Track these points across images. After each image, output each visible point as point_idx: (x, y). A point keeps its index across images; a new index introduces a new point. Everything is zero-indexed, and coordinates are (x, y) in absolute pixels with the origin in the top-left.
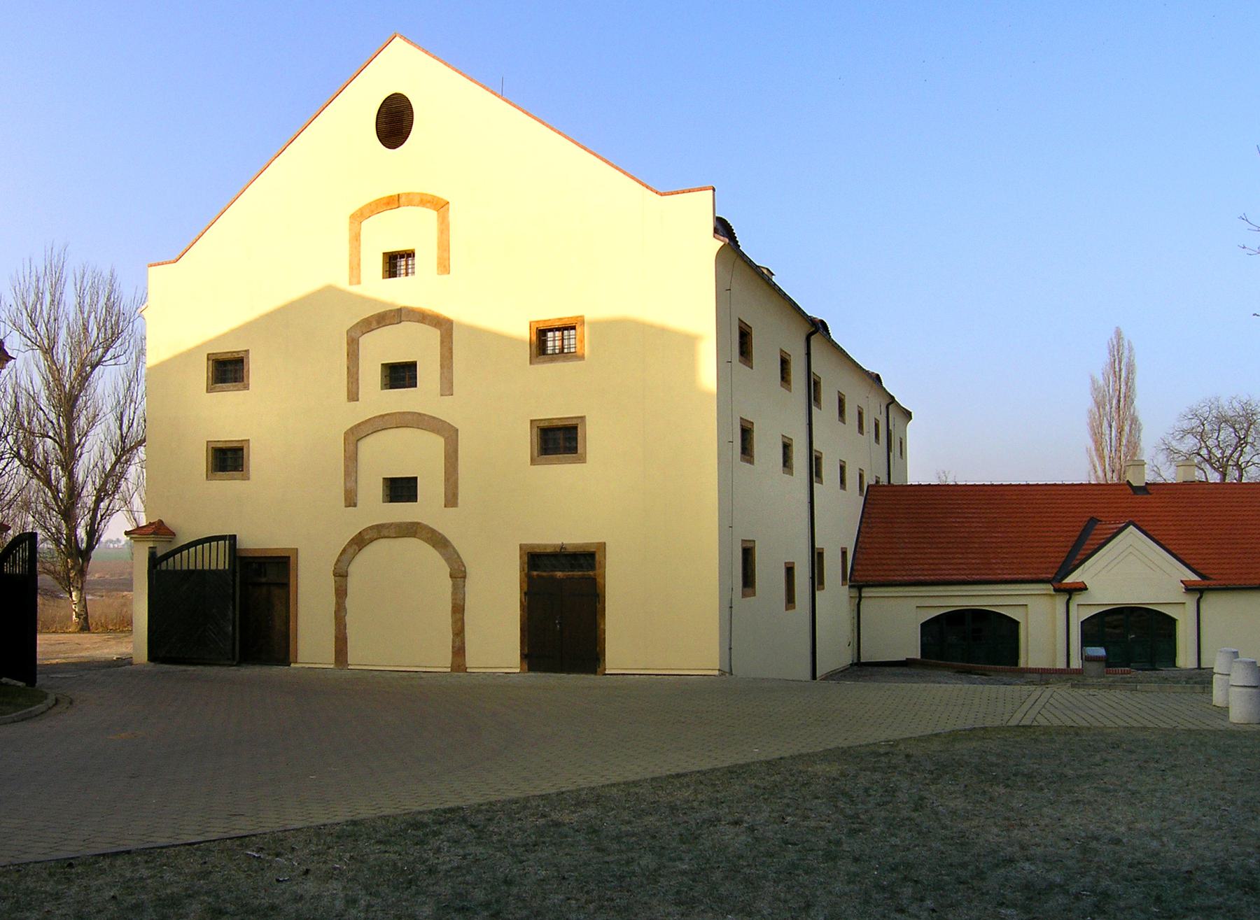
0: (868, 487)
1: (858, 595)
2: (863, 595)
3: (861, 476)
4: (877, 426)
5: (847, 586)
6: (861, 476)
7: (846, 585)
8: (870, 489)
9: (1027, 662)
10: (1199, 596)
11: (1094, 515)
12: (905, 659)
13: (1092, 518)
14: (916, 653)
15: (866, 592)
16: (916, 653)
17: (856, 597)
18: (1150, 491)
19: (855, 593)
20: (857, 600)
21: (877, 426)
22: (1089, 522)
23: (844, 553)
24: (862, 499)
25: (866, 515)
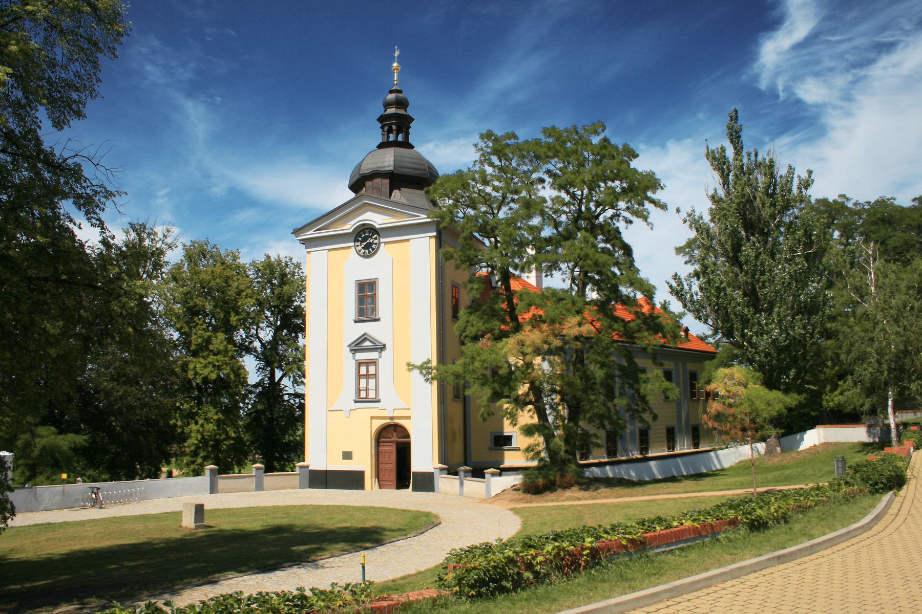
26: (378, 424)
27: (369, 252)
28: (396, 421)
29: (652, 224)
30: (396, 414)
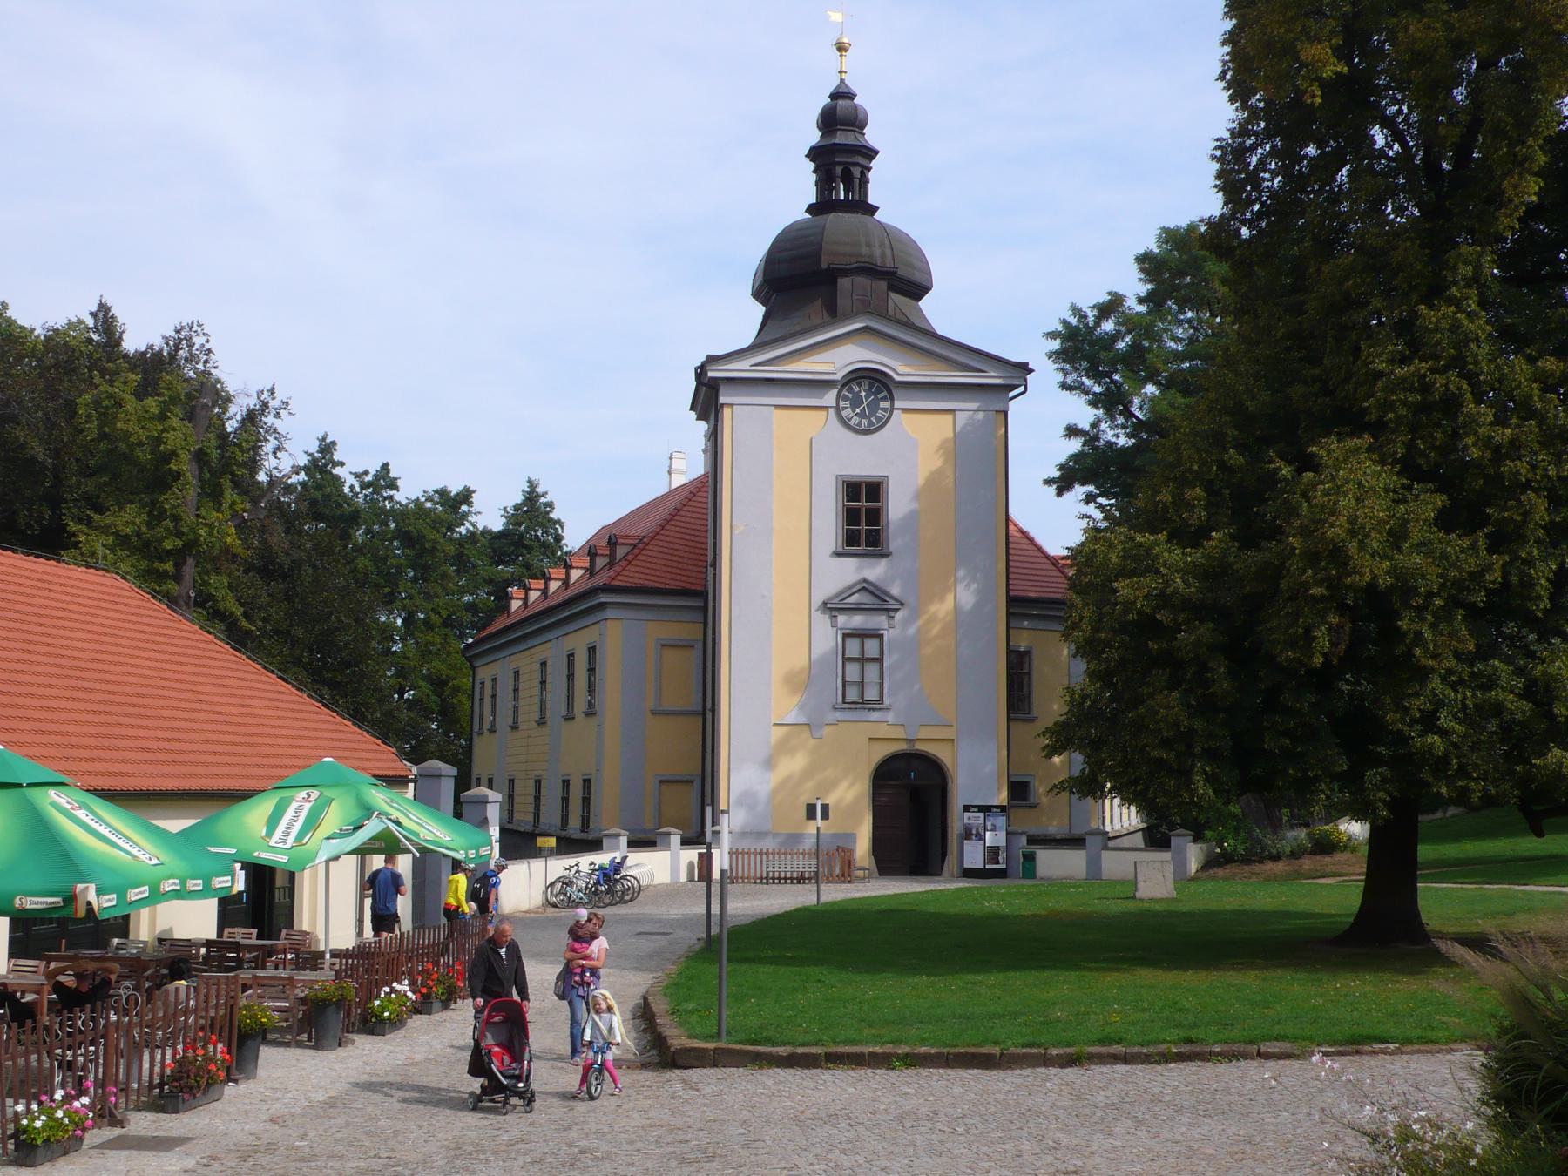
26: (883, 751)
27: (871, 424)
28: (920, 747)
29: (701, 372)
30: (923, 734)
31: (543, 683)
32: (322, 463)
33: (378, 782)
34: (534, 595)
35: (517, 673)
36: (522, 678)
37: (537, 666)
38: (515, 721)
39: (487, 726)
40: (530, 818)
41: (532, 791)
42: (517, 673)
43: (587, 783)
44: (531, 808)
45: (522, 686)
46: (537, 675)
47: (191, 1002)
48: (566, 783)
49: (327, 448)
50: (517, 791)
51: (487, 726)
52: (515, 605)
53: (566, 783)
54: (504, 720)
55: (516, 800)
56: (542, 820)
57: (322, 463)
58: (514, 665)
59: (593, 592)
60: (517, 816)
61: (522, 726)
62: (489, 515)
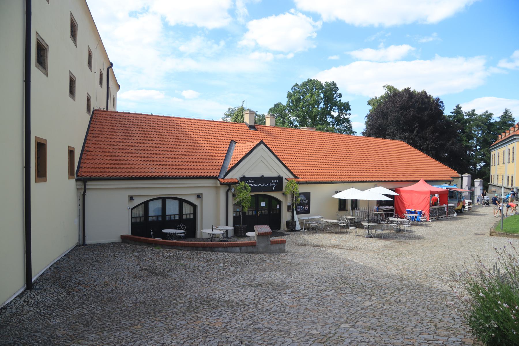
0: (94, 111)
1: (83, 187)
2: (87, 187)
3: (88, 100)
4: (101, 75)
5: (74, 180)
6: (88, 100)
7: (74, 179)
8: (95, 112)
9: (186, 212)
10: (228, 188)
11: (233, 139)
12: (260, 176)
13: (232, 141)
14: (167, 200)
15: (90, 185)
16: (167, 200)
17: (81, 189)
18: (258, 129)
19: (81, 185)
20: (83, 191)
21: (101, 75)
22: (231, 142)
23: (71, 152)
24: (89, 117)
25: (91, 129)
31: (504, 155)
32: (458, 111)
33: (358, 208)
34: (503, 136)
35: (499, 153)
36: (500, 154)
37: (503, 152)
38: (499, 163)
39: (493, 164)
40: (501, 183)
41: (502, 178)
42: (499, 153)
43: (512, 176)
44: (501, 182)
45: (500, 156)
46: (503, 153)
47: (342, 206)
48: (508, 176)
49: (458, 107)
50: (499, 178)
51: (493, 164)
52: (499, 138)
53: (508, 176)
54: (497, 163)
55: (499, 179)
56: (504, 184)
57: (458, 111)
58: (498, 151)
59: (513, 136)
60: (499, 183)
61: (500, 164)
62: (496, 118)
